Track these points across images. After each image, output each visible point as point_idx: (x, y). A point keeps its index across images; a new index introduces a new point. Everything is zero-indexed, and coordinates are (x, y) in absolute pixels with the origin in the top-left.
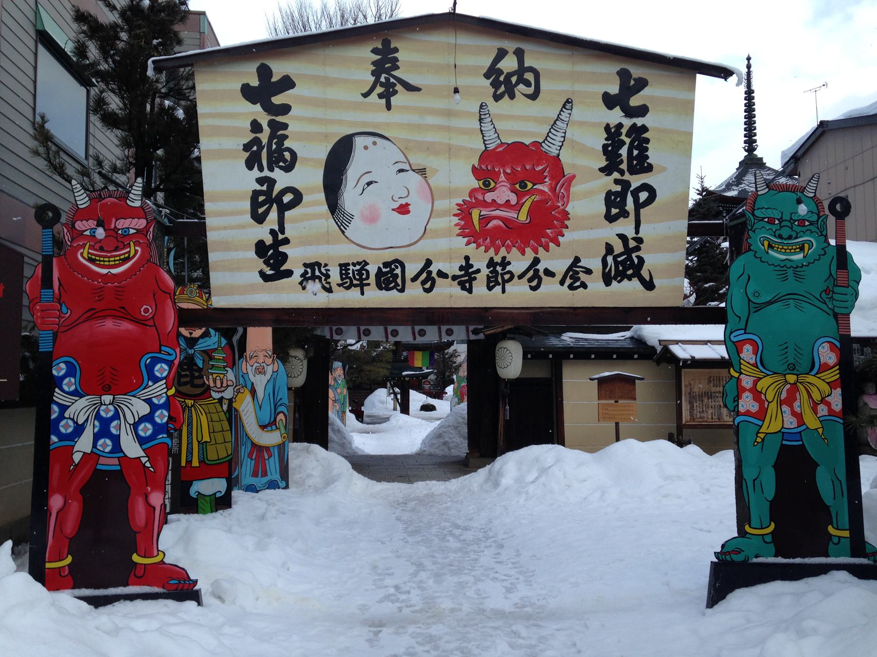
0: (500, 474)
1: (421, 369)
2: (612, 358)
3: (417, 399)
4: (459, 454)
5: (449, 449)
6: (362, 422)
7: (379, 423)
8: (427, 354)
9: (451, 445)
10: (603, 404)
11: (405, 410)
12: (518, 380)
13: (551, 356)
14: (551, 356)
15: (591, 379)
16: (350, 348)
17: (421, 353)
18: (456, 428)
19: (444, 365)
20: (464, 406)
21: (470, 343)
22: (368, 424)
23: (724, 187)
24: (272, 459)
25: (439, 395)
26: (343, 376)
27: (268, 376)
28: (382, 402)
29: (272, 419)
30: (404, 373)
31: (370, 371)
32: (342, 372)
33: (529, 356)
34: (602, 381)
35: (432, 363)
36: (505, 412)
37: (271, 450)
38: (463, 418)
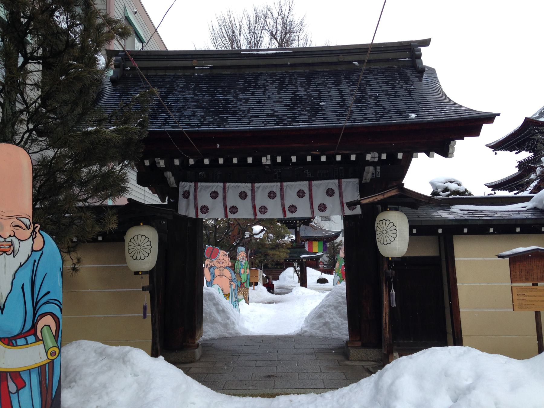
0: (392, 394)
1: (316, 253)
2: (515, 233)
3: (313, 274)
4: (340, 335)
5: (330, 330)
6: (273, 293)
7: (285, 293)
8: (322, 243)
9: (332, 326)
10: (519, 288)
11: (303, 282)
12: (403, 259)
13: (440, 231)
14: (440, 231)
15: (500, 257)
16: (255, 236)
17: (317, 242)
18: (336, 308)
19: (334, 251)
20: (343, 284)
21: (347, 219)
22: (277, 294)
23: (537, 115)
24: (25, 393)
25: (330, 272)
26: (246, 259)
27: (22, 257)
28: (291, 277)
29: (28, 326)
30: (302, 256)
31: (273, 255)
32: (245, 255)
33: (415, 231)
34: (514, 259)
35: (325, 249)
36: (390, 298)
37: (25, 377)
38: (343, 298)
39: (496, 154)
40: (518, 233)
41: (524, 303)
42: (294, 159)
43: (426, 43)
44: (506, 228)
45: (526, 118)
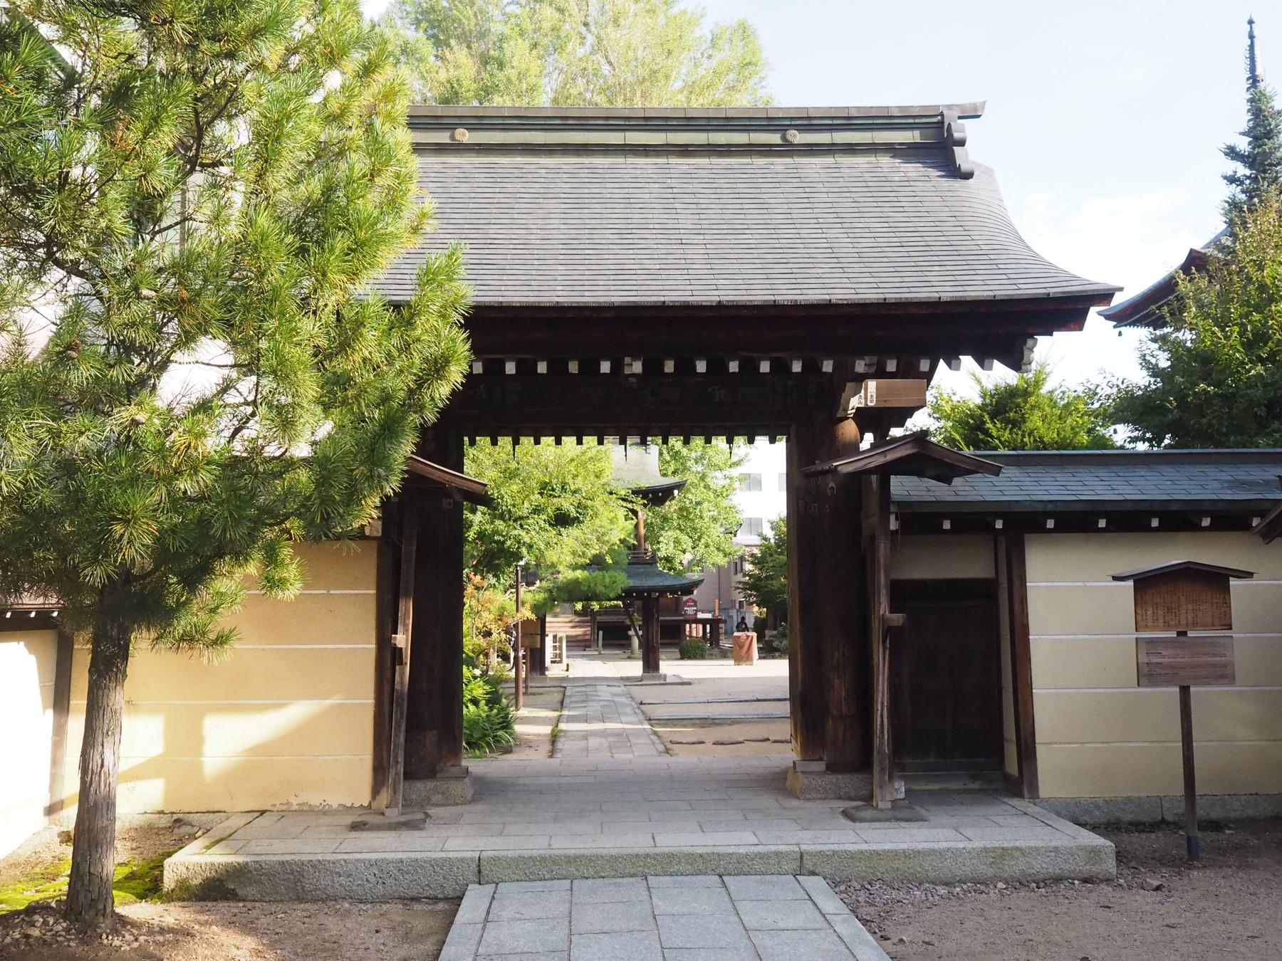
2: (1147, 528)
34: (1145, 584)
39: (1120, 334)
40: (1155, 530)
41: (1159, 671)
42: (701, 367)
43: (972, 114)
44: (1128, 521)
45: (1192, 251)
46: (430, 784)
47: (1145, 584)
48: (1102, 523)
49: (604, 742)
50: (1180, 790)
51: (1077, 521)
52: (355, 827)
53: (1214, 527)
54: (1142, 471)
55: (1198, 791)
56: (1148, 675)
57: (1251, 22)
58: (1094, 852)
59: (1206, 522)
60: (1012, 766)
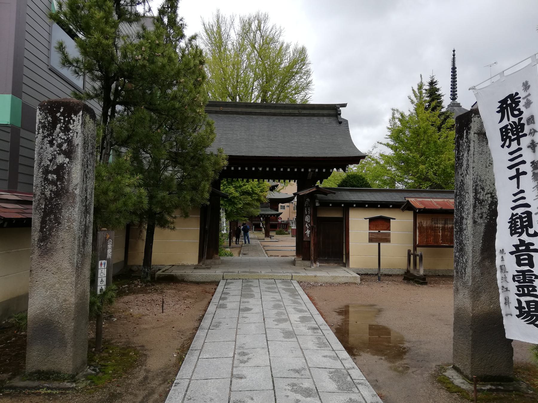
34: (371, 220)
43: (344, 105)
46: (211, 260)
47: (371, 220)
48: (367, 206)
49: (251, 38)
50: (377, 267)
51: (361, 205)
52: (195, 268)
53: (380, 207)
54: (378, 194)
55: (381, 268)
56: (371, 240)
57: (454, 51)
58: (356, 277)
59: (391, 206)
60: (344, 261)
